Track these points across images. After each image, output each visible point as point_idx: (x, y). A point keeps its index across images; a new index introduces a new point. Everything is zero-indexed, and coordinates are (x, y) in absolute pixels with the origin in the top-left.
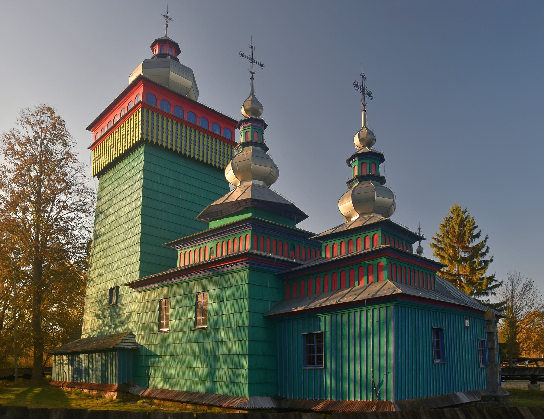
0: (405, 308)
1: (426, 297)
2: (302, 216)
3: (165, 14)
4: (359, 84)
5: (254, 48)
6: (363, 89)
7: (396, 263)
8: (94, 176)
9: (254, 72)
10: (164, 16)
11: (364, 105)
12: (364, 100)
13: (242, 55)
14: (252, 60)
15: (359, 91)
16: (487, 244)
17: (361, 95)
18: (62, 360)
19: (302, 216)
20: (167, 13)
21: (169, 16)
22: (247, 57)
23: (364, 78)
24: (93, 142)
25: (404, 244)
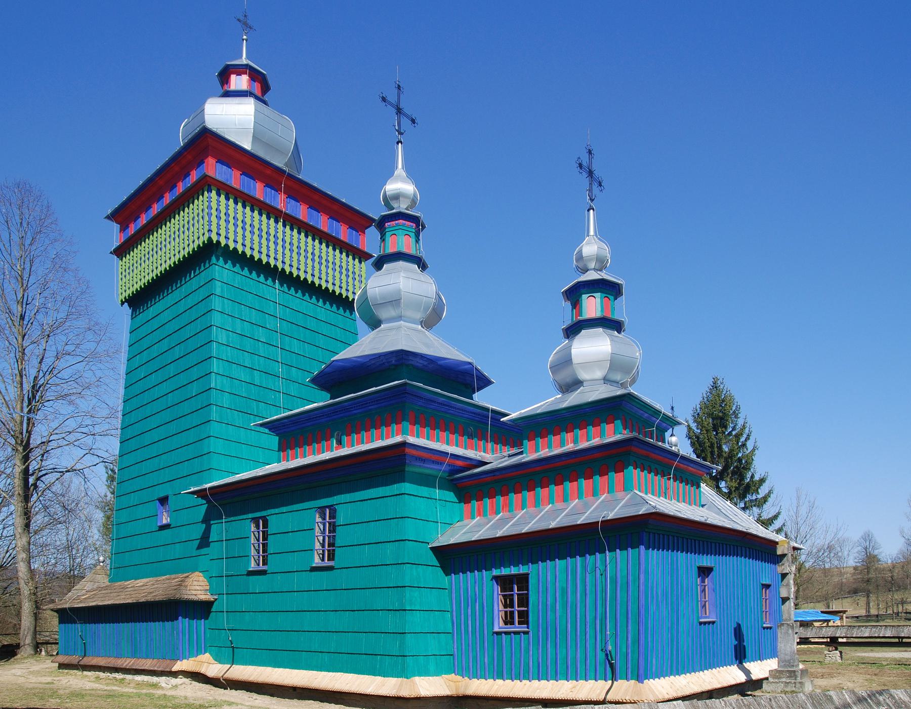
0: (649, 535)
1: (682, 516)
2: (485, 382)
3: (242, 18)
4: (584, 164)
5: (401, 89)
6: (591, 173)
7: (682, 476)
8: (123, 303)
9: (402, 131)
10: (239, 20)
11: (592, 200)
12: (590, 190)
13: (384, 99)
14: (399, 111)
15: (585, 175)
16: (747, 425)
17: (586, 181)
18: (111, 470)
19: (485, 382)
20: (245, 16)
21: (248, 21)
22: (391, 104)
23: (591, 154)
24: (601, 698)
25: (634, 424)
